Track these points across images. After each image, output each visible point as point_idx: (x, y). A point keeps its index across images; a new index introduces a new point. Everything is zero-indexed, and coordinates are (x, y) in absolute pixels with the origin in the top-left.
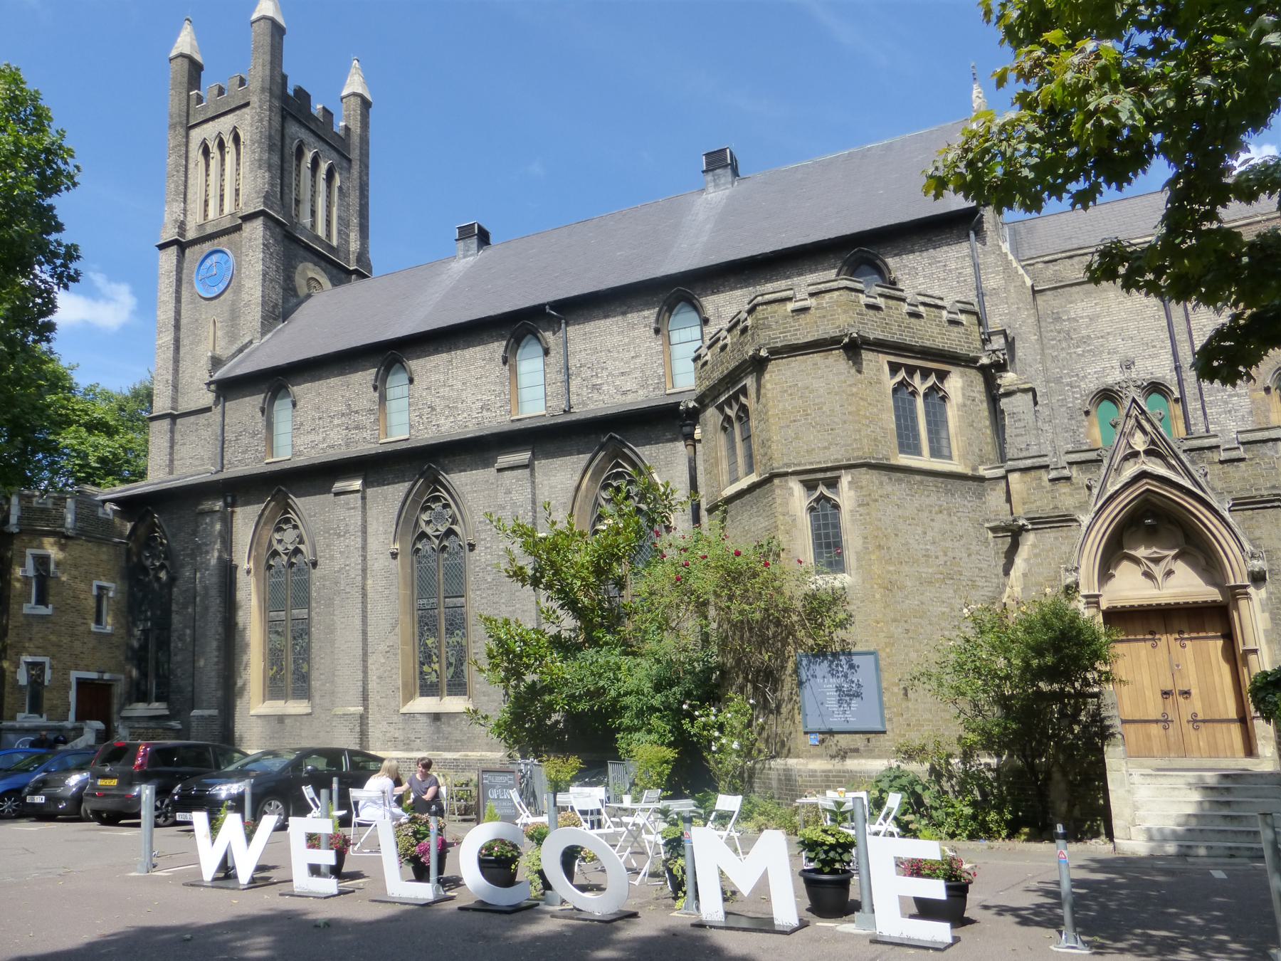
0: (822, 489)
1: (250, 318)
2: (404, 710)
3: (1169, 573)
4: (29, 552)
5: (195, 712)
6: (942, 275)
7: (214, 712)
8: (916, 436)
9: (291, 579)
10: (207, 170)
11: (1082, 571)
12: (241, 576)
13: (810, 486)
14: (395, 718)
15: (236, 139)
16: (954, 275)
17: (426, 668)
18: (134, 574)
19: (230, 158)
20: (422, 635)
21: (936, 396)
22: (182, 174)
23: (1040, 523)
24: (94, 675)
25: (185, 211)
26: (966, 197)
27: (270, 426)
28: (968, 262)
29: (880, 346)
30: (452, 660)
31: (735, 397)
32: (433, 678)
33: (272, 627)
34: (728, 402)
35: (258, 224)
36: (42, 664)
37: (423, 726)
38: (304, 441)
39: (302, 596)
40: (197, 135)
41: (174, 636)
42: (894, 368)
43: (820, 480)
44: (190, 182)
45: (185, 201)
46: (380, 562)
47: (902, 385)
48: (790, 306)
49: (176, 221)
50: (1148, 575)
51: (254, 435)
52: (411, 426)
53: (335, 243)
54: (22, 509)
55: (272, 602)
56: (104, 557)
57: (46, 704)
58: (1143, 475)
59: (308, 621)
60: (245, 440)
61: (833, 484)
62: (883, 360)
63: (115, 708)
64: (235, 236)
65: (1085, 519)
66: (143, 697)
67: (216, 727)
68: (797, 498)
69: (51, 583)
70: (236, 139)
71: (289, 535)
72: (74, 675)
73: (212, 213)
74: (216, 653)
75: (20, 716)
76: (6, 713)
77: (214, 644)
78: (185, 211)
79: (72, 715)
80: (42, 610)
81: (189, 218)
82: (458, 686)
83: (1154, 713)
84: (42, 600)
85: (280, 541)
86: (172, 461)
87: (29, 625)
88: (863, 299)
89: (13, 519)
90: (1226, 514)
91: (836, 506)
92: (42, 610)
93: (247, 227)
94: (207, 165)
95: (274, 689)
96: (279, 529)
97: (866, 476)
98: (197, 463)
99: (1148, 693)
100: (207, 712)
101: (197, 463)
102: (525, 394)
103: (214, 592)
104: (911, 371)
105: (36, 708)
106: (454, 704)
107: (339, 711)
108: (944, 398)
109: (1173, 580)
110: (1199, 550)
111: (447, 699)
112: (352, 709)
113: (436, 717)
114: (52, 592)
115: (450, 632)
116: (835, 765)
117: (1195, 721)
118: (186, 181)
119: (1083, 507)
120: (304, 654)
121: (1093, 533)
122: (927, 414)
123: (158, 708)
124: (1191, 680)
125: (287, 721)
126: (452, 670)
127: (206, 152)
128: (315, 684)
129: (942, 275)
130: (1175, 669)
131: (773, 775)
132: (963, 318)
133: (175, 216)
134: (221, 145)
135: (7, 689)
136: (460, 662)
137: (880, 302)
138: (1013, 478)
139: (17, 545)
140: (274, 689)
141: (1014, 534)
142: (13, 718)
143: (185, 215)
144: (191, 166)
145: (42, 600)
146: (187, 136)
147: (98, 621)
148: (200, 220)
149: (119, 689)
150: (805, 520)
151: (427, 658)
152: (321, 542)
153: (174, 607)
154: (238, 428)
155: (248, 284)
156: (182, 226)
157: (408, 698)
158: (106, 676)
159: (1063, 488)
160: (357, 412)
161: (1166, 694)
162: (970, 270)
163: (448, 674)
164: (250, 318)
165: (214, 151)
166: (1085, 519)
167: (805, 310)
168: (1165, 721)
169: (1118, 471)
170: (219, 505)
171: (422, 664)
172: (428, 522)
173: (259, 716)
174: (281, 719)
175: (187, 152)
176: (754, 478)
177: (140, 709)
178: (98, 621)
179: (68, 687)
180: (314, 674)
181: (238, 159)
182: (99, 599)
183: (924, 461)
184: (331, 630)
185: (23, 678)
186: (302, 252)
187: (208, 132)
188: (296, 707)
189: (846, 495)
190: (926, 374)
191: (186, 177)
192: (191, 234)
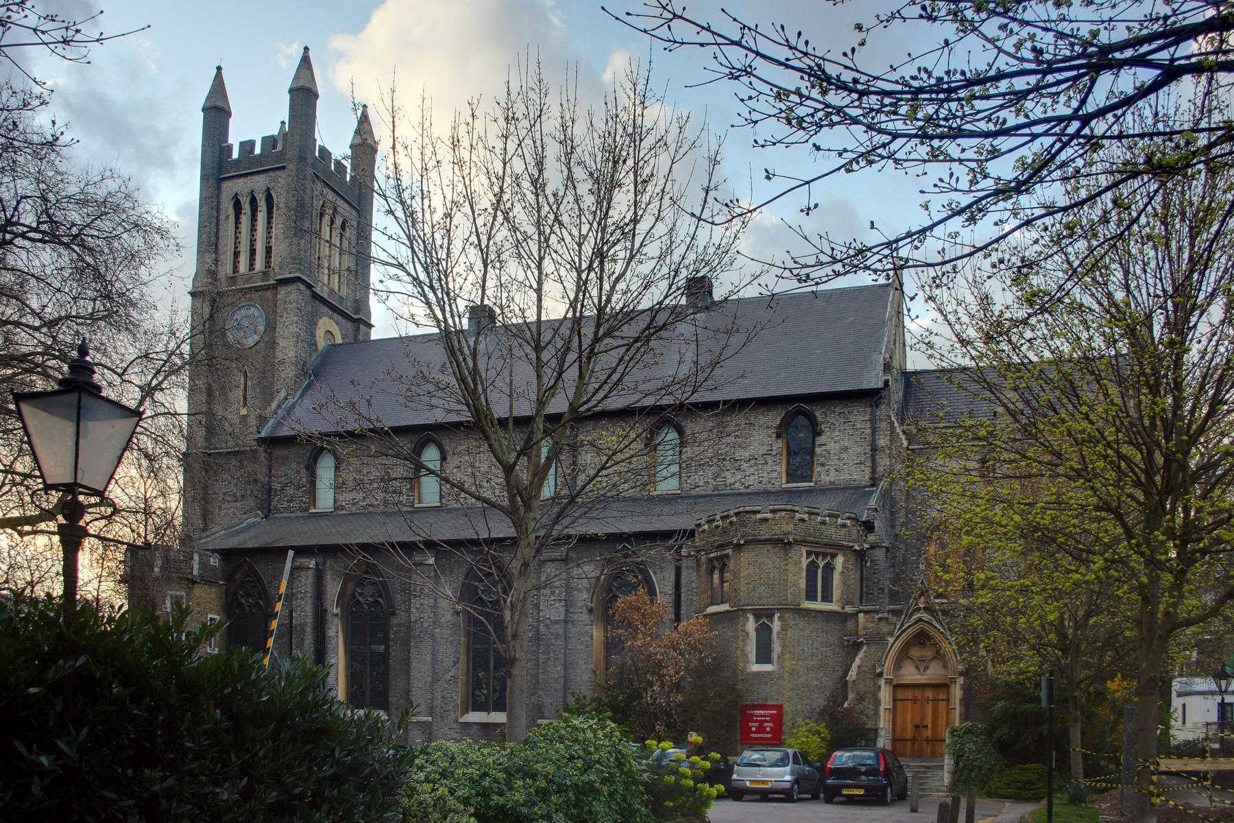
1: (283, 375)
6: (851, 432)
8: (816, 591)
12: (329, 618)
13: (758, 616)
14: (454, 726)
15: (269, 199)
16: (859, 432)
17: (477, 692)
19: (262, 217)
20: (474, 669)
21: (829, 568)
22: (213, 225)
25: (216, 261)
27: (313, 483)
28: (868, 425)
29: (803, 542)
30: (498, 688)
31: (722, 557)
34: (717, 558)
38: (345, 497)
40: (229, 189)
42: (809, 554)
43: (764, 615)
44: (222, 233)
45: (216, 251)
46: (446, 617)
47: (813, 562)
48: (759, 516)
49: (209, 271)
50: (917, 667)
51: (298, 487)
52: (441, 497)
53: (344, 293)
56: (213, 596)
58: (920, 620)
59: (386, 656)
60: (290, 491)
62: (804, 550)
64: (269, 294)
65: (891, 640)
68: (751, 625)
70: (269, 199)
73: (243, 267)
78: (216, 261)
81: (220, 268)
85: (360, 594)
88: (798, 515)
91: (770, 629)
93: (283, 291)
97: (788, 616)
98: (229, 499)
99: (909, 726)
101: (229, 499)
103: (309, 629)
104: (817, 555)
106: (499, 717)
107: (414, 719)
108: (833, 569)
109: (929, 672)
111: (493, 714)
118: (217, 232)
119: (891, 634)
120: (384, 677)
122: (823, 577)
126: (497, 694)
129: (851, 432)
132: (848, 522)
133: (207, 266)
137: (806, 516)
138: (861, 615)
141: (857, 646)
143: (216, 265)
144: (223, 217)
146: (218, 188)
148: (229, 271)
150: (753, 635)
155: (282, 343)
156: (213, 274)
159: (883, 623)
160: (395, 479)
161: (917, 727)
162: (868, 431)
164: (283, 375)
165: (246, 208)
168: (913, 740)
169: (910, 616)
171: (474, 689)
172: (483, 591)
175: (219, 203)
176: (725, 607)
180: (391, 693)
181: (269, 222)
183: (819, 605)
184: (407, 662)
186: (324, 309)
187: (241, 186)
189: (776, 625)
190: (825, 555)
191: (218, 229)
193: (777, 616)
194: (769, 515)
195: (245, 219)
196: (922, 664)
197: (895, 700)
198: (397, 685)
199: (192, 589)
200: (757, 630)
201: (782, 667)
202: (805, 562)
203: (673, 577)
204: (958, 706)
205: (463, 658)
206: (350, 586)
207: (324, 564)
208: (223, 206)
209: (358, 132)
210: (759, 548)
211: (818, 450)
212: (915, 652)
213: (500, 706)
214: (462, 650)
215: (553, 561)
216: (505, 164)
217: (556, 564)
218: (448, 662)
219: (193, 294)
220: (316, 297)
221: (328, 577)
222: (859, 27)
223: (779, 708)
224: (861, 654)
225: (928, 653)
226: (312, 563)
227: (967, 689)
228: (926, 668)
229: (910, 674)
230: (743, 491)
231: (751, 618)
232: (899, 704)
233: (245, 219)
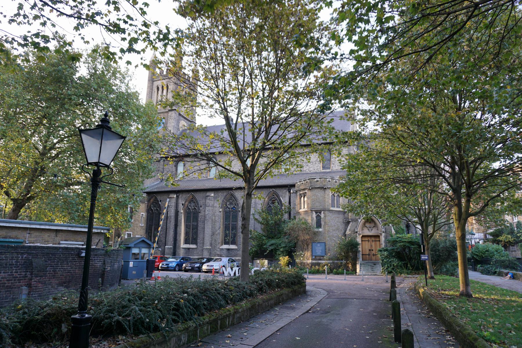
0: (318, 213)
7: (172, 247)
9: (193, 217)
10: (158, 92)
13: (316, 213)
14: (218, 250)
23: (353, 220)
26: (355, 46)
32: (228, 240)
33: (187, 227)
35: (173, 112)
37: (225, 251)
55: (187, 220)
61: (320, 213)
67: (172, 250)
82: (233, 243)
83: (367, 253)
88: (328, 180)
94: (158, 92)
95: (186, 242)
96: (190, 203)
97: (326, 212)
100: (170, 247)
107: (205, 247)
109: (373, 231)
110: (375, 226)
111: (231, 246)
113: (228, 249)
115: (232, 230)
116: (320, 261)
117: (373, 255)
119: (360, 219)
120: (196, 233)
121: (361, 221)
124: (373, 248)
127: (158, 88)
130: (371, 246)
131: (426, 255)
134: (163, 87)
136: (234, 237)
140: (186, 242)
141: (349, 222)
146: (153, 84)
151: (226, 236)
154: (168, 170)
161: (370, 250)
163: (231, 240)
166: (359, 220)
167: (318, 181)
168: (369, 255)
174: (189, 249)
180: (198, 238)
184: (204, 228)
186: (182, 118)
187: (159, 83)
188: (194, 246)
189: (322, 215)
193: (322, 212)
194: (319, 180)
195: (160, 92)
198: (200, 236)
201: (325, 229)
202: (331, 194)
203: (288, 200)
204: (383, 243)
205: (222, 227)
208: (154, 89)
210: (316, 190)
211: (332, 160)
212: (368, 225)
213: (194, 241)
220: (180, 115)
223: (325, 243)
224: (350, 225)
225: (372, 225)
226: (175, 196)
227: (386, 237)
229: (367, 232)
230: (309, 172)
231: (314, 213)
233: (160, 92)
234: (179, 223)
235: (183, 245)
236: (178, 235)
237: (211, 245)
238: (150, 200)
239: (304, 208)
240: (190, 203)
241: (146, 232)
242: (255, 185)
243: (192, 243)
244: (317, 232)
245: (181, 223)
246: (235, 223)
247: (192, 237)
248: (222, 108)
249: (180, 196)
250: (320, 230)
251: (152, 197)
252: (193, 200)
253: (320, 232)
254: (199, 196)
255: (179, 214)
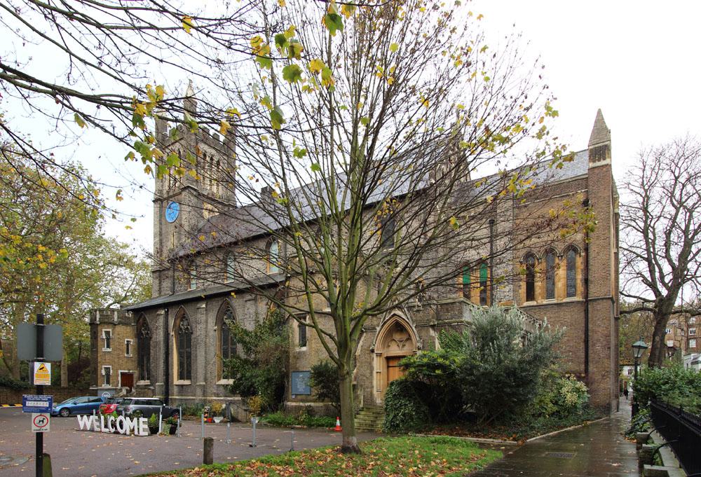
2: (217, 383)
3: (224, 371)
4: (103, 330)
5: (157, 384)
7: (162, 384)
9: (186, 339)
11: (376, 346)
18: (139, 335)
24: (127, 371)
33: (180, 355)
36: (109, 368)
39: (189, 346)
41: (151, 358)
46: (212, 333)
54: (101, 315)
55: (180, 347)
57: (111, 381)
63: (134, 382)
65: (378, 329)
66: (143, 378)
69: (111, 341)
71: (185, 323)
72: (120, 371)
74: (286, 81)
75: (103, 385)
76: (99, 384)
77: (163, 361)
79: (120, 385)
80: (109, 350)
84: (108, 347)
86: (160, 288)
87: (105, 355)
89: (98, 319)
90: (414, 328)
92: (109, 350)
93: (184, 193)
95: (181, 377)
96: (182, 320)
102: (212, 326)
103: (162, 343)
105: (108, 382)
107: (198, 384)
109: (405, 348)
111: (186, 381)
112: (202, 383)
114: (111, 343)
119: (378, 326)
120: (189, 365)
121: (381, 331)
123: (147, 382)
125: (184, 387)
128: (192, 375)
135: (99, 377)
139: (99, 328)
140: (181, 377)
142: (101, 386)
145: (108, 347)
147: (128, 353)
149: (136, 376)
152: (194, 325)
153: (151, 348)
157: (219, 379)
158: (131, 371)
166: (378, 329)
170: (163, 312)
173: (176, 385)
174: (182, 386)
177: (142, 383)
178: (128, 353)
179: (118, 376)
182: (128, 345)
185: (103, 372)
188: (187, 382)
192: (165, 196)
196: (402, 343)
197: (388, 367)
199: (114, 328)
200: (299, 326)
201: (311, 348)
206: (178, 321)
207: (168, 311)
209: (597, 116)
213: (189, 378)
214: (218, 348)
215: (249, 300)
216: (506, 116)
217: (251, 302)
218: (212, 354)
219: (154, 201)
221: (170, 318)
222: (480, 17)
225: (405, 337)
226: (163, 312)
228: (404, 346)
232: (391, 369)
234: (170, 350)
235: (176, 381)
236: (170, 368)
237: (206, 380)
238: (139, 320)
239: (550, 293)
240: (182, 320)
241: (139, 364)
242: (308, 277)
243: (187, 379)
244: (299, 353)
245: (173, 350)
246: (234, 346)
247: (186, 372)
248: (394, 73)
249: (170, 310)
250: (304, 349)
251: (140, 317)
252: (183, 317)
253: (304, 352)
254: (189, 310)
255: (170, 337)
